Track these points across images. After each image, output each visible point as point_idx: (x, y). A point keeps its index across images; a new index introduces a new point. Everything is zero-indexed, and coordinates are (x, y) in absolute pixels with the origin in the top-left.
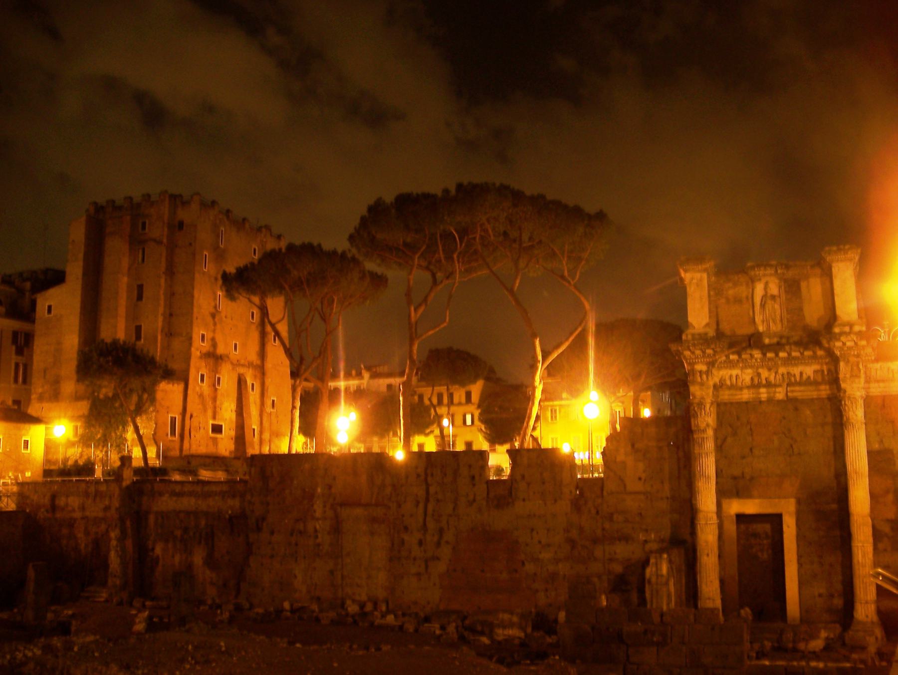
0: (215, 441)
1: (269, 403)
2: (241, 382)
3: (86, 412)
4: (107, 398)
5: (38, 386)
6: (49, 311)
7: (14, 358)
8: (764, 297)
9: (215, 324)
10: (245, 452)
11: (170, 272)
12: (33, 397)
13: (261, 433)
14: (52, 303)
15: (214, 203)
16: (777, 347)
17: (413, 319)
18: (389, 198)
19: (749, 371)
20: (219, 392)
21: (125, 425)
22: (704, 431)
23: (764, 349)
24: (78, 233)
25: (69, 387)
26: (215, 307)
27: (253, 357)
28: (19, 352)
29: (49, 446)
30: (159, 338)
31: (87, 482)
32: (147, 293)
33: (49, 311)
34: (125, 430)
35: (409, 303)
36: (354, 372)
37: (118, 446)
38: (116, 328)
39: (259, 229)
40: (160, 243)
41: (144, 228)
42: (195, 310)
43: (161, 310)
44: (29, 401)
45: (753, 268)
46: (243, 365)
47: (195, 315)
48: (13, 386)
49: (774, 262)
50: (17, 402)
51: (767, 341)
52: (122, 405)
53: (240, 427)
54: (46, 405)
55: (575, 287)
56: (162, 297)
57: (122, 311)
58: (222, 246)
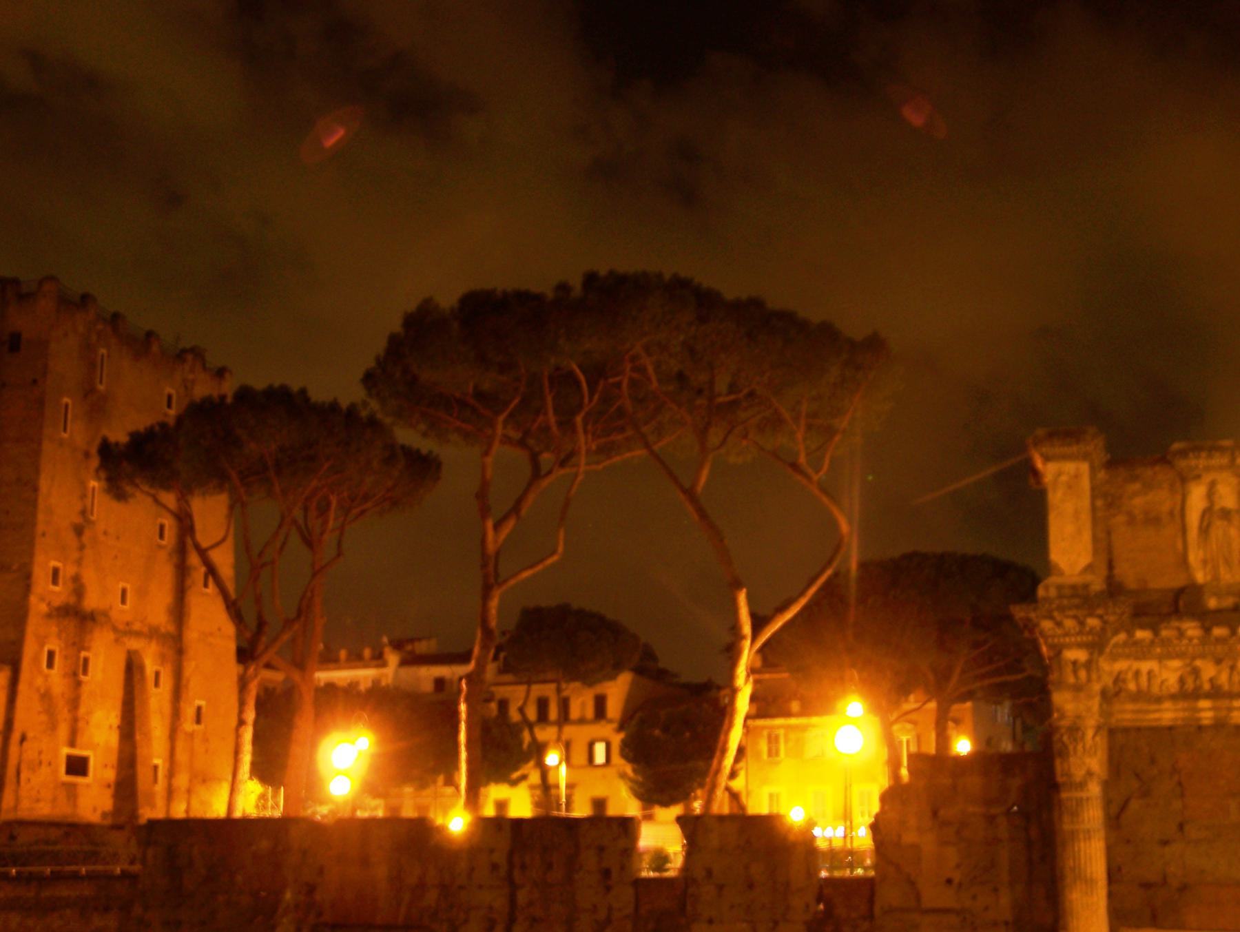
0: (71, 791)
1: (189, 712)
2: (132, 669)
8: (1207, 512)
9: (82, 548)
13: (171, 774)
15: (86, 299)
17: (491, 547)
19: (1176, 663)
20: (85, 689)
22: (1082, 785)
23: (1207, 619)
35: (485, 512)
36: (367, 653)
39: (181, 356)
42: (41, 517)
45: (1183, 453)
46: (138, 634)
47: (41, 527)
51: (1212, 603)
53: (128, 761)
58: (101, 388)
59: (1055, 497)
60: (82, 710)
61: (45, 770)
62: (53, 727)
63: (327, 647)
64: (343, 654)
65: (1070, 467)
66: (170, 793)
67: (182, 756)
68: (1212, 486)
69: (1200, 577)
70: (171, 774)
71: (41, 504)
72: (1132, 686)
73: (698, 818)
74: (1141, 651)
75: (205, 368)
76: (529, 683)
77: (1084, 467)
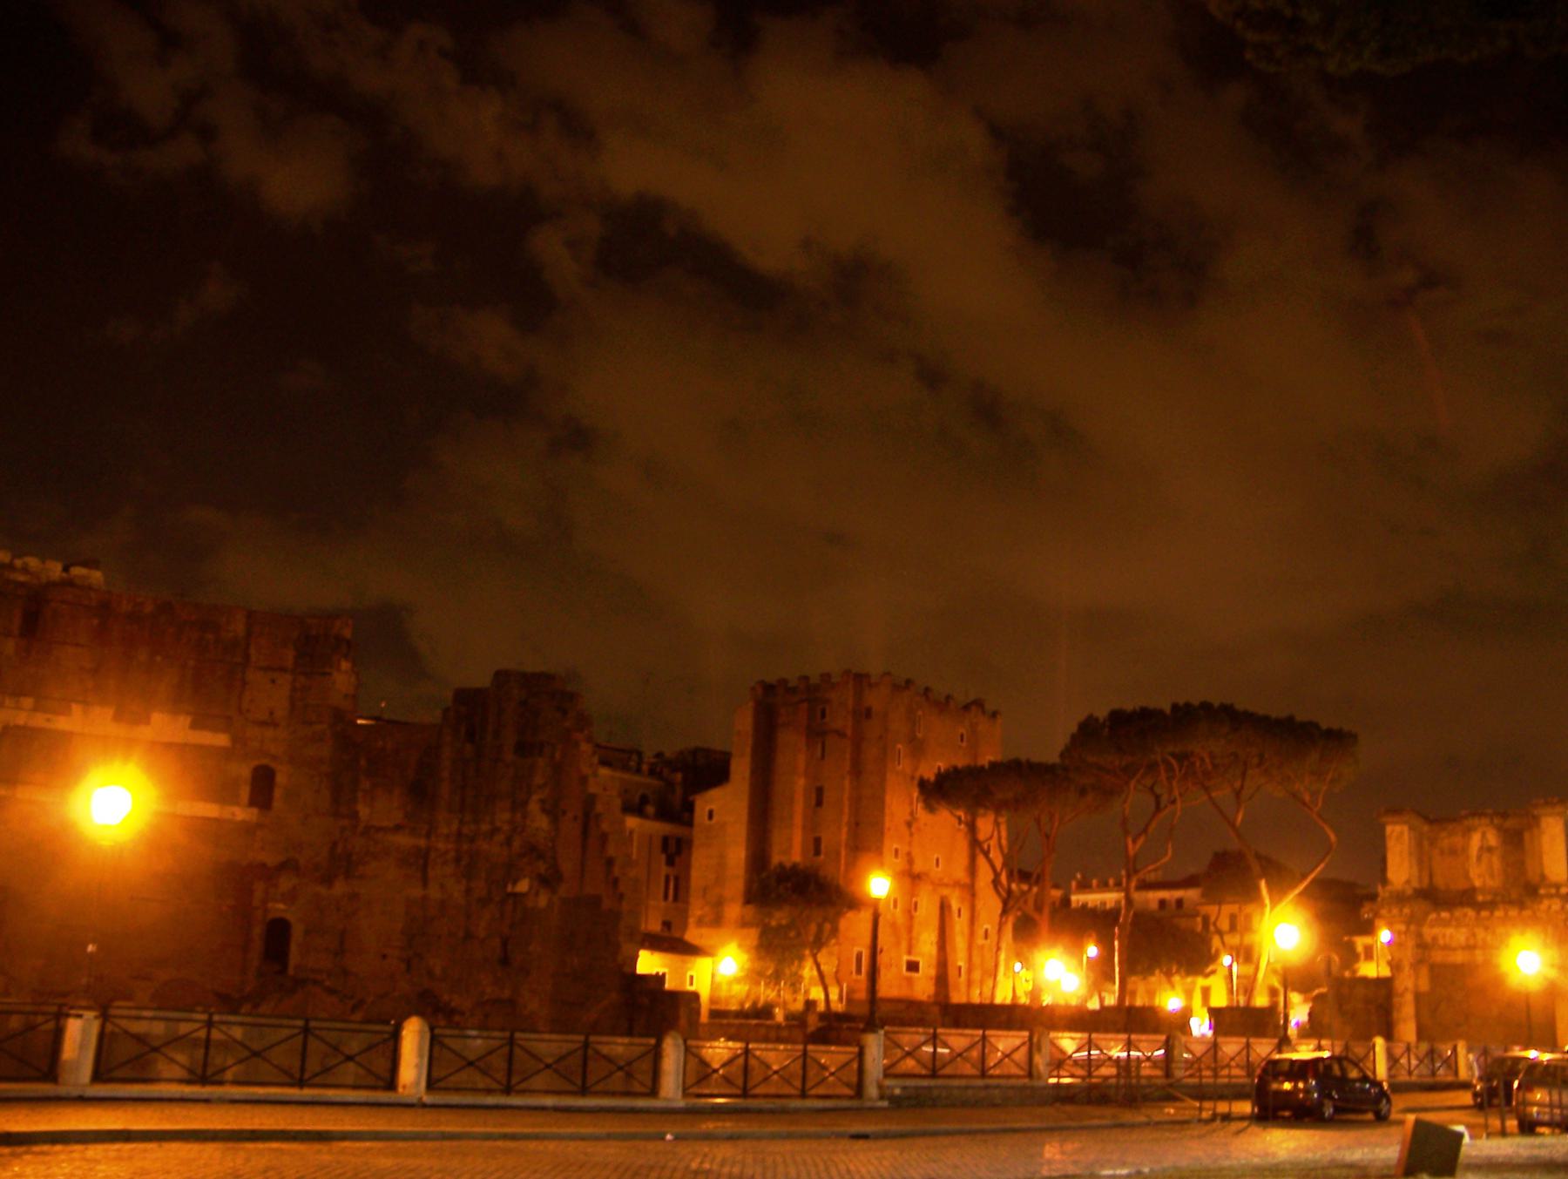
0: (910, 981)
1: (980, 933)
2: (944, 907)
3: (755, 943)
4: (780, 927)
5: (697, 909)
6: (711, 815)
7: (665, 870)
8: (1481, 848)
9: (911, 835)
10: (947, 996)
11: (857, 771)
12: (691, 920)
13: (970, 971)
14: (713, 807)
15: (909, 682)
16: (1491, 905)
17: (1131, 852)
18: (1102, 713)
19: (1464, 930)
20: (916, 921)
21: (801, 959)
22: (1402, 995)
23: (1478, 907)
24: (745, 722)
25: (734, 910)
26: (912, 814)
27: (960, 873)
28: (670, 862)
29: (715, 986)
30: (843, 853)
31: (769, 1027)
32: (828, 796)
33: (711, 815)
34: (801, 967)
35: (1126, 833)
36: (1111, 882)
37: (793, 985)
38: (790, 849)
39: (966, 708)
40: (841, 734)
41: (823, 716)
42: (887, 819)
43: (846, 818)
44: (685, 926)
45: (1466, 817)
46: (947, 885)
47: (887, 825)
48: (663, 904)
49: (1489, 811)
50: (667, 925)
51: (1480, 898)
52: (799, 934)
53: (943, 964)
54: (704, 931)
55: (1320, 816)
56: (847, 803)
57: (798, 819)
58: (919, 735)
59: (1391, 843)
60: (915, 934)
61: (894, 969)
62: (898, 944)
63: (1083, 877)
64: (1094, 882)
65: (1398, 828)
66: (969, 983)
67: (976, 960)
68: (1484, 835)
69: (1477, 883)
70: (970, 971)
71: (887, 811)
72: (1441, 942)
73: (1261, 1011)
74: (1446, 924)
75: (984, 712)
76: (1220, 904)
77: (1406, 828)
